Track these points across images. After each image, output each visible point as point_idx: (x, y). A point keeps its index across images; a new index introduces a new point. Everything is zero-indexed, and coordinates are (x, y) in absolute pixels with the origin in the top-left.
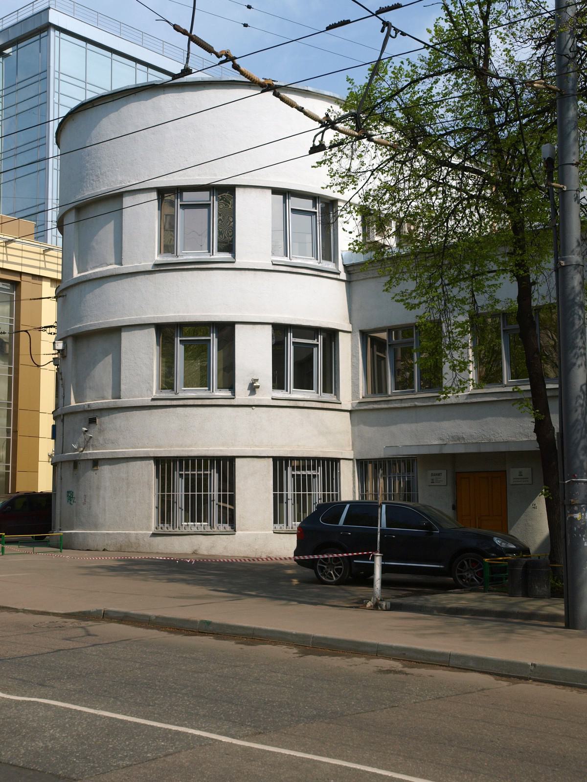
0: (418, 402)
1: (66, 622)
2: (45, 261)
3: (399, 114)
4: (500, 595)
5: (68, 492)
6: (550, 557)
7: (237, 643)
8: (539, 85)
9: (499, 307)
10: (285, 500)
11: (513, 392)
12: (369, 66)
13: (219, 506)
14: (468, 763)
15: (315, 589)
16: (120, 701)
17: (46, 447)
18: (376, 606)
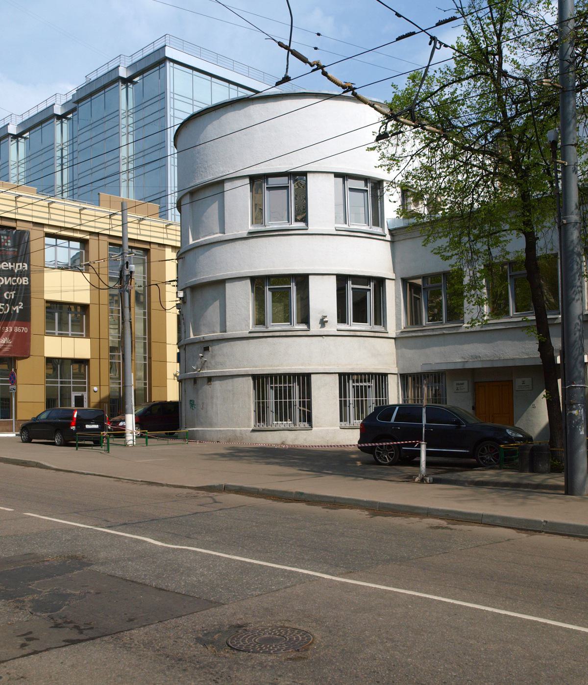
0: (445, 331)
1: (198, 493)
2: (167, 233)
3: (431, 112)
4: (512, 471)
5: (191, 401)
6: (550, 443)
7: (323, 508)
8: (547, 84)
9: (511, 257)
10: (348, 405)
11: (522, 321)
12: (408, 75)
13: (300, 410)
14: (508, 593)
15: (374, 469)
16: (246, 549)
17: (173, 368)
18: (422, 481)
